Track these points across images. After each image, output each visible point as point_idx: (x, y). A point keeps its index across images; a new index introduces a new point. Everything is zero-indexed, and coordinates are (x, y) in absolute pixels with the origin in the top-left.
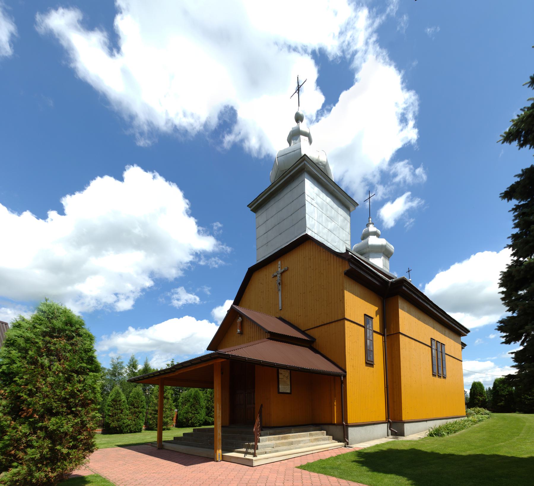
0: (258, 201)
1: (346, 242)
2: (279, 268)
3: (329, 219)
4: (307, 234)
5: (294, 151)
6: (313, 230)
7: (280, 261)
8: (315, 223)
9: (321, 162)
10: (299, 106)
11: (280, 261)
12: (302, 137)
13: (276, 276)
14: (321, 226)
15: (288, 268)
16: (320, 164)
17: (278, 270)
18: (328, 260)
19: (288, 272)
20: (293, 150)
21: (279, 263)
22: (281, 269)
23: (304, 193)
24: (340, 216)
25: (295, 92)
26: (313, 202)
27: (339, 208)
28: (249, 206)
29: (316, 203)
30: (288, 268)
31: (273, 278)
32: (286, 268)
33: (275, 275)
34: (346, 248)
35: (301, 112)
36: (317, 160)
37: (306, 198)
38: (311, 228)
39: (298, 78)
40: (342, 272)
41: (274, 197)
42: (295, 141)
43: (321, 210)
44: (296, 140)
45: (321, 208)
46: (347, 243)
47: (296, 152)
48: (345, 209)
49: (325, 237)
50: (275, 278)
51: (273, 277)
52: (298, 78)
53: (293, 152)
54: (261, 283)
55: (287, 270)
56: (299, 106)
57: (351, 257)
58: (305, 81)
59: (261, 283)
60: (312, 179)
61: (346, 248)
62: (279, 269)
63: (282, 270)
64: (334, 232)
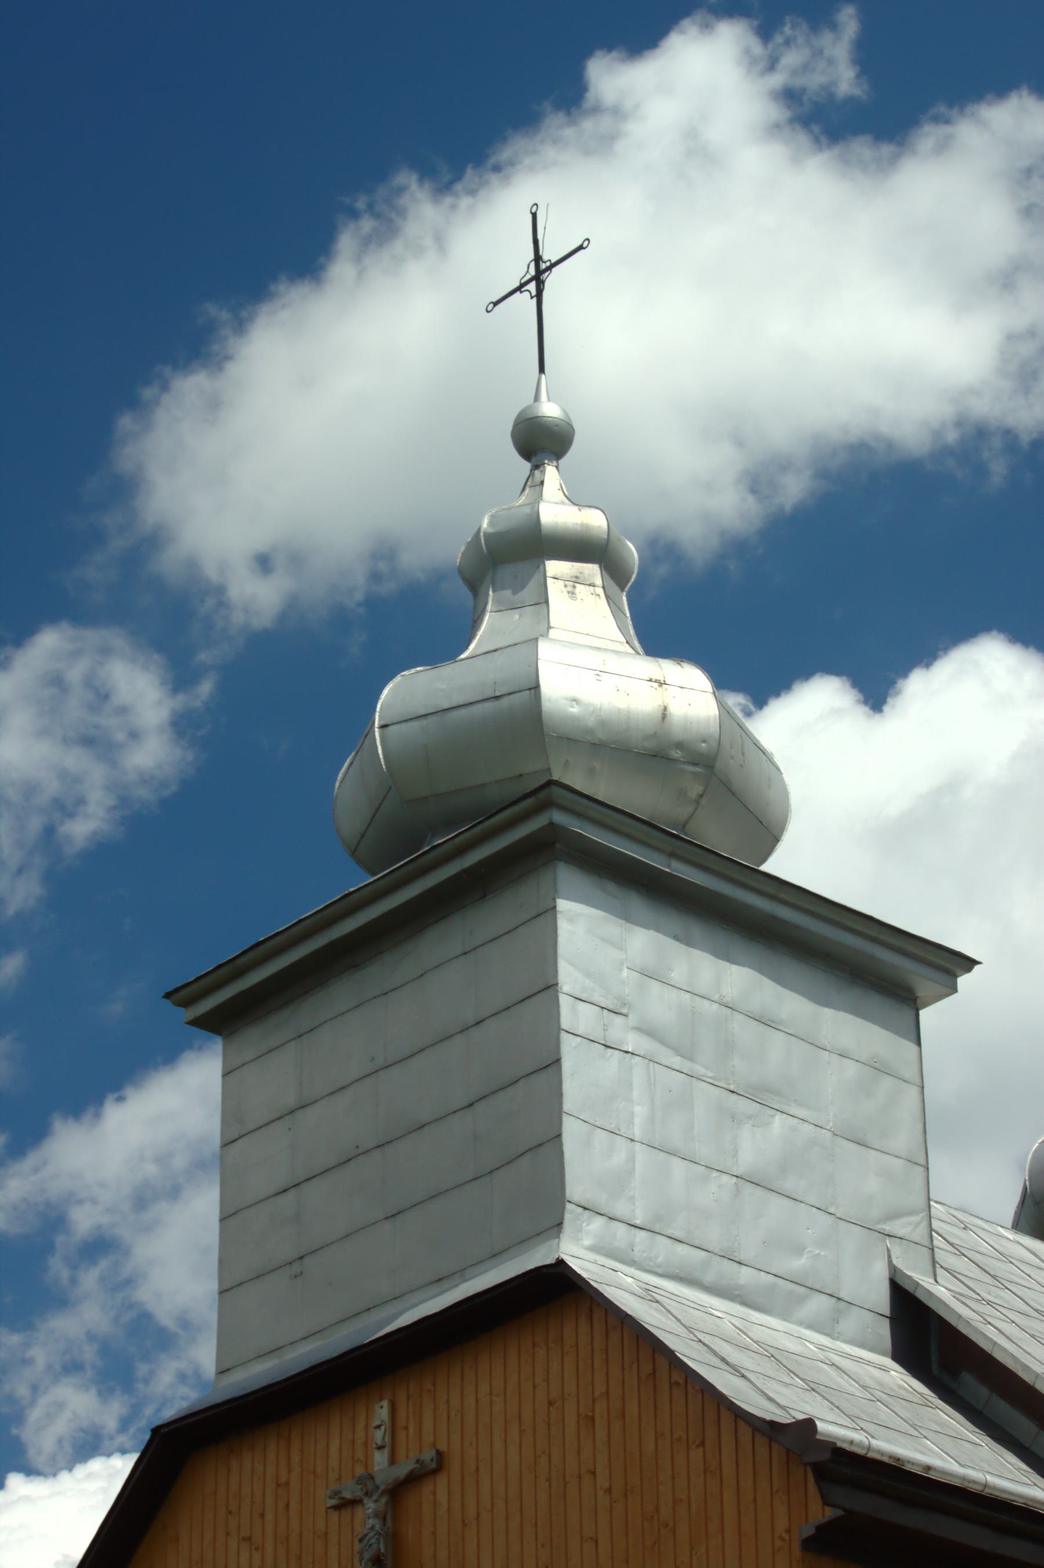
0: (240, 973)
1: (887, 1228)
2: (380, 1448)
3: (743, 1105)
4: (561, 1263)
5: (497, 698)
6: (621, 1209)
7: (385, 1403)
8: (632, 1158)
9: (679, 745)
10: (542, 369)
11: (385, 1403)
12: (554, 567)
13: (354, 1502)
14: (678, 1167)
15: (440, 1454)
16: (676, 754)
17: (367, 1462)
18: (702, 1444)
19: (440, 1487)
20: (490, 693)
21: (382, 1412)
22: (392, 1461)
23: (551, 987)
24: (835, 1058)
25: (519, 289)
26: (620, 1031)
27: (827, 1012)
28: (176, 997)
29: (638, 1029)
30: (440, 1454)
31: (334, 1515)
32: (428, 1455)
33: (348, 1495)
34: (893, 1270)
35: (550, 410)
36: (655, 735)
37: (566, 1020)
38: (601, 1199)
39: (534, 216)
40: (788, 1531)
41: (356, 966)
42: (507, 593)
43: (677, 1061)
44: (519, 586)
45: (677, 1051)
46: (900, 1233)
47: (504, 702)
48: (876, 1002)
49: (714, 1236)
50: (346, 1513)
51: (337, 1508)
52: (534, 216)
53: (489, 706)
54: (248, 1539)
55: (435, 1472)
56: (542, 369)
57: (826, 1456)
58: (581, 248)
59: (248, 1539)
60: (611, 886)
61: (893, 1270)
62: (380, 1459)
63: (403, 1470)
64: (790, 1184)
